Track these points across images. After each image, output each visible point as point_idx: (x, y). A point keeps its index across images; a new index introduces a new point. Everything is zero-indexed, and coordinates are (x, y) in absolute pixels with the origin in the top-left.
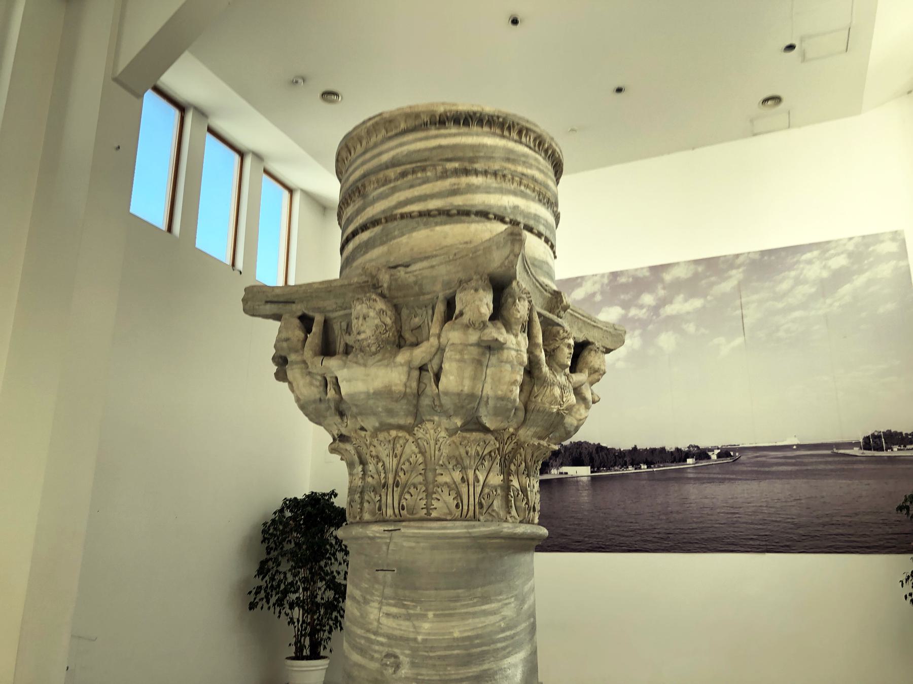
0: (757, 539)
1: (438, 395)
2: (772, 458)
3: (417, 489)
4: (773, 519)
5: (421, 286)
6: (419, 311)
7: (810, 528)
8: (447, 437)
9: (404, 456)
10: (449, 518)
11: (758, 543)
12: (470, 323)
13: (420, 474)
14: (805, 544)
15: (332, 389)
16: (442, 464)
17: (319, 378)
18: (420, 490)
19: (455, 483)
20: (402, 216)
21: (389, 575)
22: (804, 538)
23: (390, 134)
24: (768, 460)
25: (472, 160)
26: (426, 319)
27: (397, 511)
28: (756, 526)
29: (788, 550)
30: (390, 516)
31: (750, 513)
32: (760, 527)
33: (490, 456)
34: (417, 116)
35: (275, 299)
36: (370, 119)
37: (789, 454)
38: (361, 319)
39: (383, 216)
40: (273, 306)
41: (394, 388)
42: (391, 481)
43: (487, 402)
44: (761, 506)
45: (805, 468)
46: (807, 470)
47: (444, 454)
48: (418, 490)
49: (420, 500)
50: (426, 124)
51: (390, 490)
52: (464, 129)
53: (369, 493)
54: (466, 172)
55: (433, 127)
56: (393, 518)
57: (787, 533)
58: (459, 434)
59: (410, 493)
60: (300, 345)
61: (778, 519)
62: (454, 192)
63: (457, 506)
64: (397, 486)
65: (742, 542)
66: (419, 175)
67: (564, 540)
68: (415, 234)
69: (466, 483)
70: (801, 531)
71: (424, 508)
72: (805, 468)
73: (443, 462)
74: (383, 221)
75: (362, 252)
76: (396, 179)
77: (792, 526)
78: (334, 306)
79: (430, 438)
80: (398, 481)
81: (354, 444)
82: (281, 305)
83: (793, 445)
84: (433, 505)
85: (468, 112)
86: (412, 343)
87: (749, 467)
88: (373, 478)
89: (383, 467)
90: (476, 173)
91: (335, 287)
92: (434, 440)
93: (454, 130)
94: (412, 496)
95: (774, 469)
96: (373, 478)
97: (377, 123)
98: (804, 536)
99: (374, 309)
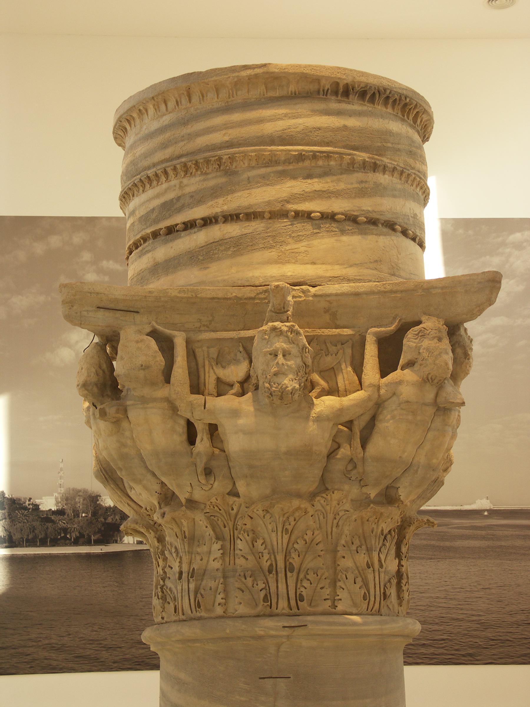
0: (430, 646)
1: (363, 459)
2: (455, 528)
3: (317, 576)
4: (454, 616)
5: (334, 315)
6: (332, 349)
7: (500, 630)
8: (352, 510)
9: (296, 532)
10: (354, 611)
11: (432, 650)
12: (428, 379)
13: (319, 556)
14: (494, 652)
15: (205, 438)
16: (345, 544)
17: (183, 423)
18: (321, 576)
19: (357, 568)
20: (298, 215)
21: (282, 684)
22: (492, 643)
23: (271, 94)
24: (450, 530)
25: (381, 151)
26: (343, 360)
27: (293, 603)
28: (430, 626)
29: (471, 661)
30: (283, 609)
31: (423, 608)
32: (436, 627)
33: (391, 535)
34: (317, 80)
35: (112, 306)
36: (246, 67)
37: (478, 522)
38: (280, 356)
39: (268, 209)
40: (107, 314)
41: (315, 448)
42: (281, 564)
43: (417, 471)
44: (437, 598)
45: (499, 543)
46: (501, 546)
47: (346, 532)
48: (319, 577)
49: (322, 588)
50: (325, 93)
51: (281, 575)
52: (367, 107)
53: (243, 579)
54: (375, 167)
55: (333, 98)
56: (287, 611)
57: (472, 636)
58: (372, 508)
59: (308, 580)
60: (161, 378)
61: (461, 617)
62: (362, 193)
63: (365, 598)
64: (292, 571)
65: (410, 649)
66: (320, 163)
67: (141, 651)
68: (316, 242)
69: (372, 569)
70: (489, 634)
71: (328, 599)
72: (499, 543)
73: (346, 541)
74: (267, 215)
75: (230, 253)
76: (288, 161)
77: (478, 626)
78: (197, 325)
79: (329, 512)
80: (290, 563)
81: (205, 513)
82: (118, 314)
83: (485, 510)
84: (338, 595)
85: (378, 87)
86: (323, 388)
87: (424, 539)
88: (247, 559)
89: (264, 545)
90: (384, 169)
91: (202, 299)
92: (333, 514)
93: (356, 107)
94: (311, 584)
95: (459, 543)
96: (247, 559)
97: (256, 76)
98: (493, 640)
99: (298, 345)
